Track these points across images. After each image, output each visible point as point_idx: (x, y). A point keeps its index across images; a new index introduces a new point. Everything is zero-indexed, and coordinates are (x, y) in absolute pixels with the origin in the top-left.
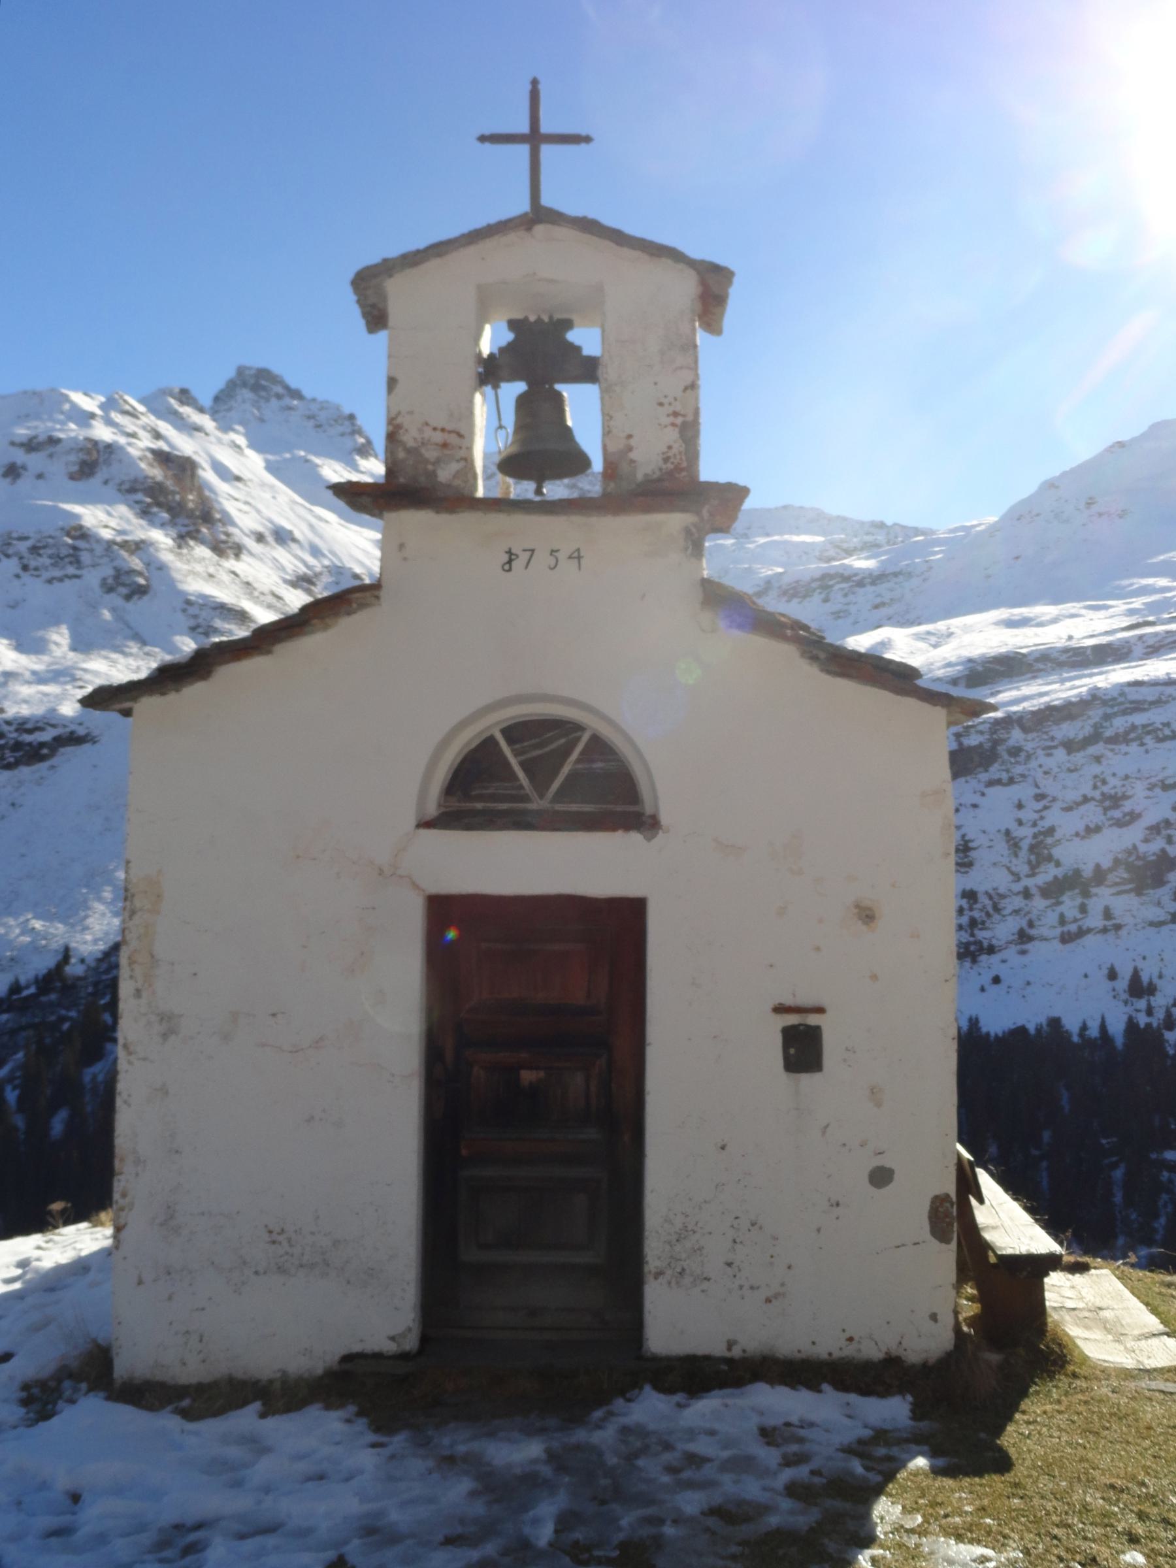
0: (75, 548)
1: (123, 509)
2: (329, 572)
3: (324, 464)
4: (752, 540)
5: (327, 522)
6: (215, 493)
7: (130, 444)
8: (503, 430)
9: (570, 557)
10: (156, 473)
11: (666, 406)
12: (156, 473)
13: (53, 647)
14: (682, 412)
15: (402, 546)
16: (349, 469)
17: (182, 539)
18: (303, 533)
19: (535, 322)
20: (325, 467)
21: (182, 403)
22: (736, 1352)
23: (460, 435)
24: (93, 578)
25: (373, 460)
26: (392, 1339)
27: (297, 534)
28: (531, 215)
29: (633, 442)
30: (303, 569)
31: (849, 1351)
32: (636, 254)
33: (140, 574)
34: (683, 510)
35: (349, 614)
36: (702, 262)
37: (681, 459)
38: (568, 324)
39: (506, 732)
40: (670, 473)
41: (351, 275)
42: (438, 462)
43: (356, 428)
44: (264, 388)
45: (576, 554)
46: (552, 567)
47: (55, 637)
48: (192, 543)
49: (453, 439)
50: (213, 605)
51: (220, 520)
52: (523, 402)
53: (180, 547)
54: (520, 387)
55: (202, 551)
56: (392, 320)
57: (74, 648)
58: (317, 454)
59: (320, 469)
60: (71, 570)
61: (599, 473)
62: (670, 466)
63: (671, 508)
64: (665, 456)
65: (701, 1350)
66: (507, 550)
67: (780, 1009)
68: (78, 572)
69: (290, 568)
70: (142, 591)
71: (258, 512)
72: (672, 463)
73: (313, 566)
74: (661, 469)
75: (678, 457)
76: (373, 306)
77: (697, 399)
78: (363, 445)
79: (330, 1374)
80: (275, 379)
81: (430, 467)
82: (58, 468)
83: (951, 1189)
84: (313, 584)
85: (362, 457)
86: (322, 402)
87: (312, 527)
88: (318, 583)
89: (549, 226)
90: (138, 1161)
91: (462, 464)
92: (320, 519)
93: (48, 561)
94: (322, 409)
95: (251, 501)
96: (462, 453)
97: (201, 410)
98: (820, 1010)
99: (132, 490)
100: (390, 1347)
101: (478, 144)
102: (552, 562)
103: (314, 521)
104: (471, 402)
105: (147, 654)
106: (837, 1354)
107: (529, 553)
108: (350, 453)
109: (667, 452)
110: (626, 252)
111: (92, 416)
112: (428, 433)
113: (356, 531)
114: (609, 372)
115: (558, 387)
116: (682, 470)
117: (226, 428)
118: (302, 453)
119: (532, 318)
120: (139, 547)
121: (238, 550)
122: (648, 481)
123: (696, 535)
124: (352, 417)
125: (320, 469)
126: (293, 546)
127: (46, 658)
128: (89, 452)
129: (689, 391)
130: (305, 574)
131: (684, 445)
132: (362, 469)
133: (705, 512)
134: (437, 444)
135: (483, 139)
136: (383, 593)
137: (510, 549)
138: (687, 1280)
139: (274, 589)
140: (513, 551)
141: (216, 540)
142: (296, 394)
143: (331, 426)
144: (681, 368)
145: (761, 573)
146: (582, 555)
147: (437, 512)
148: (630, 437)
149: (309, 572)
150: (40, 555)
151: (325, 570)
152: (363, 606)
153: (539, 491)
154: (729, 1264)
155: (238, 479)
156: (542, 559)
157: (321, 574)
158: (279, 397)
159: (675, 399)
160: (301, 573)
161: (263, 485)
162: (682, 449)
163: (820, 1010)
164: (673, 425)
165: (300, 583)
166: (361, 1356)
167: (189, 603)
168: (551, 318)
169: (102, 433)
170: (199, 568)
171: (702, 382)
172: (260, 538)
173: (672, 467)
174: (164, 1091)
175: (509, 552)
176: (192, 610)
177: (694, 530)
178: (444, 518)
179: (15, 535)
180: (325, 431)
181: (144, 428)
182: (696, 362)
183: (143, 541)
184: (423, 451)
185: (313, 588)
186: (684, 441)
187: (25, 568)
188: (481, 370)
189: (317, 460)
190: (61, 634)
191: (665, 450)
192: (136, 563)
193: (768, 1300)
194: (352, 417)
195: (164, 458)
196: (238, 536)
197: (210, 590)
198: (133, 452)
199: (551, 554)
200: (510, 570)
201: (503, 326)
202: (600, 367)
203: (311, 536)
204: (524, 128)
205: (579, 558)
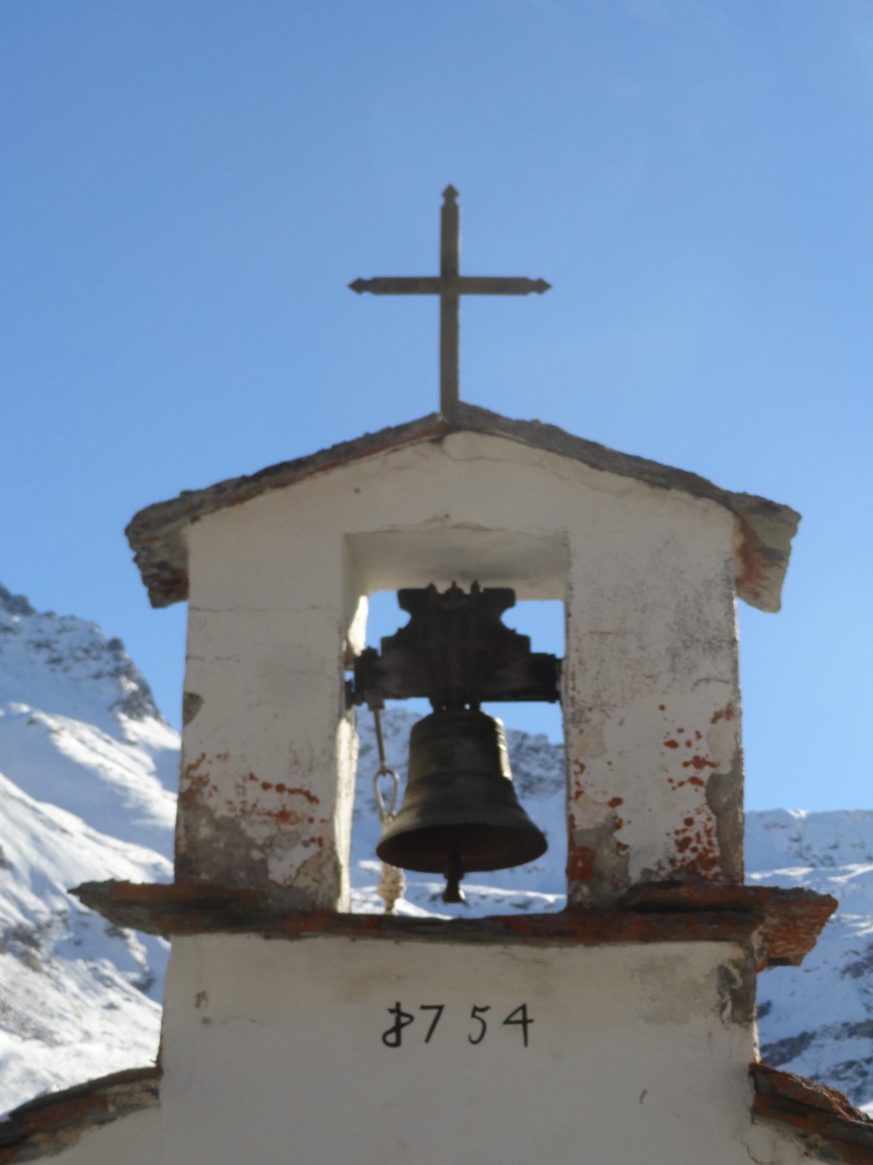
2: (65, 921)
3: (63, 729)
4: (841, 868)
5: (64, 831)
8: (388, 776)
9: (507, 1022)
11: (682, 747)
14: (711, 759)
15: (201, 997)
16: (107, 737)
18: (20, 851)
19: (449, 593)
20: (66, 734)
23: (312, 799)
25: (150, 720)
27: (10, 854)
28: (440, 419)
29: (621, 812)
30: (16, 917)
32: (629, 482)
35: (102, 1122)
36: (744, 497)
37: (710, 843)
38: (507, 599)
40: (691, 868)
41: (126, 518)
42: (269, 844)
43: (122, 664)
45: (519, 1016)
46: (475, 1037)
49: (298, 805)
56: (193, 590)
58: (51, 711)
59: (54, 736)
61: (558, 747)
63: (695, 936)
64: (681, 837)
66: (393, 1006)
72: (694, 850)
73: (36, 912)
74: (672, 861)
75: (704, 839)
76: (163, 565)
77: (737, 735)
78: (134, 694)
81: (256, 855)
84: (36, 945)
85: (131, 717)
86: (63, 619)
87: (35, 839)
88: (42, 942)
89: (472, 436)
91: (314, 848)
94: (62, 630)
96: (315, 830)
101: (352, 294)
102: (475, 1028)
103: (40, 829)
104: (333, 738)
107: (434, 1012)
108: (111, 709)
109: (684, 831)
110: (608, 478)
112: (253, 792)
113: (115, 849)
115: (488, 708)
116: (713, 862)
118: (25, 708)
119: (442, 588)
122: (648, 884)
123: (740, 982)
124: (115, 645)
125: (54, 736)
129: (721, 721)
130: (20, 926)
131: (714, 817)
132: (132, 738)
133: (756, 940)
134: (269, 814)
135: (359, 286)
136: (164, 1085)
137: (398, 1005)
140: (404, 1009)
142: (20, 605)
143: (77, 660)
144: (707, 680)
145: (861, 929)
146: (529, 1017)
147: (267, 937)
148: (616, 802)
149: (27, 922)
151: (57, 918)
152: (125, 1109)
153: (451, 895)
157: (49, 925)
159: (699, 736)
160: (13, 923)
162: (711, 825)
164: (695, 781)
165: (11, 942)
168: (475, 587)
171: (746, 705)
173: (692, 856)
175: (397, 1011)
177: (735, 973)
178: (281, 947)
180: (66, 670)
182: (735, 669)
184: (244, 825)
185: (33, 951)
186: (715, 811)
188: (349, 675)
189: (51, 722)
191: (681, 826)
194: (115, 645)
199: (473, 1016)
200: (398, 1043)
201: (390, 598)
202: (563, 678)
203: (33, 856)
204: (432, 269)
205: (525, 1022)
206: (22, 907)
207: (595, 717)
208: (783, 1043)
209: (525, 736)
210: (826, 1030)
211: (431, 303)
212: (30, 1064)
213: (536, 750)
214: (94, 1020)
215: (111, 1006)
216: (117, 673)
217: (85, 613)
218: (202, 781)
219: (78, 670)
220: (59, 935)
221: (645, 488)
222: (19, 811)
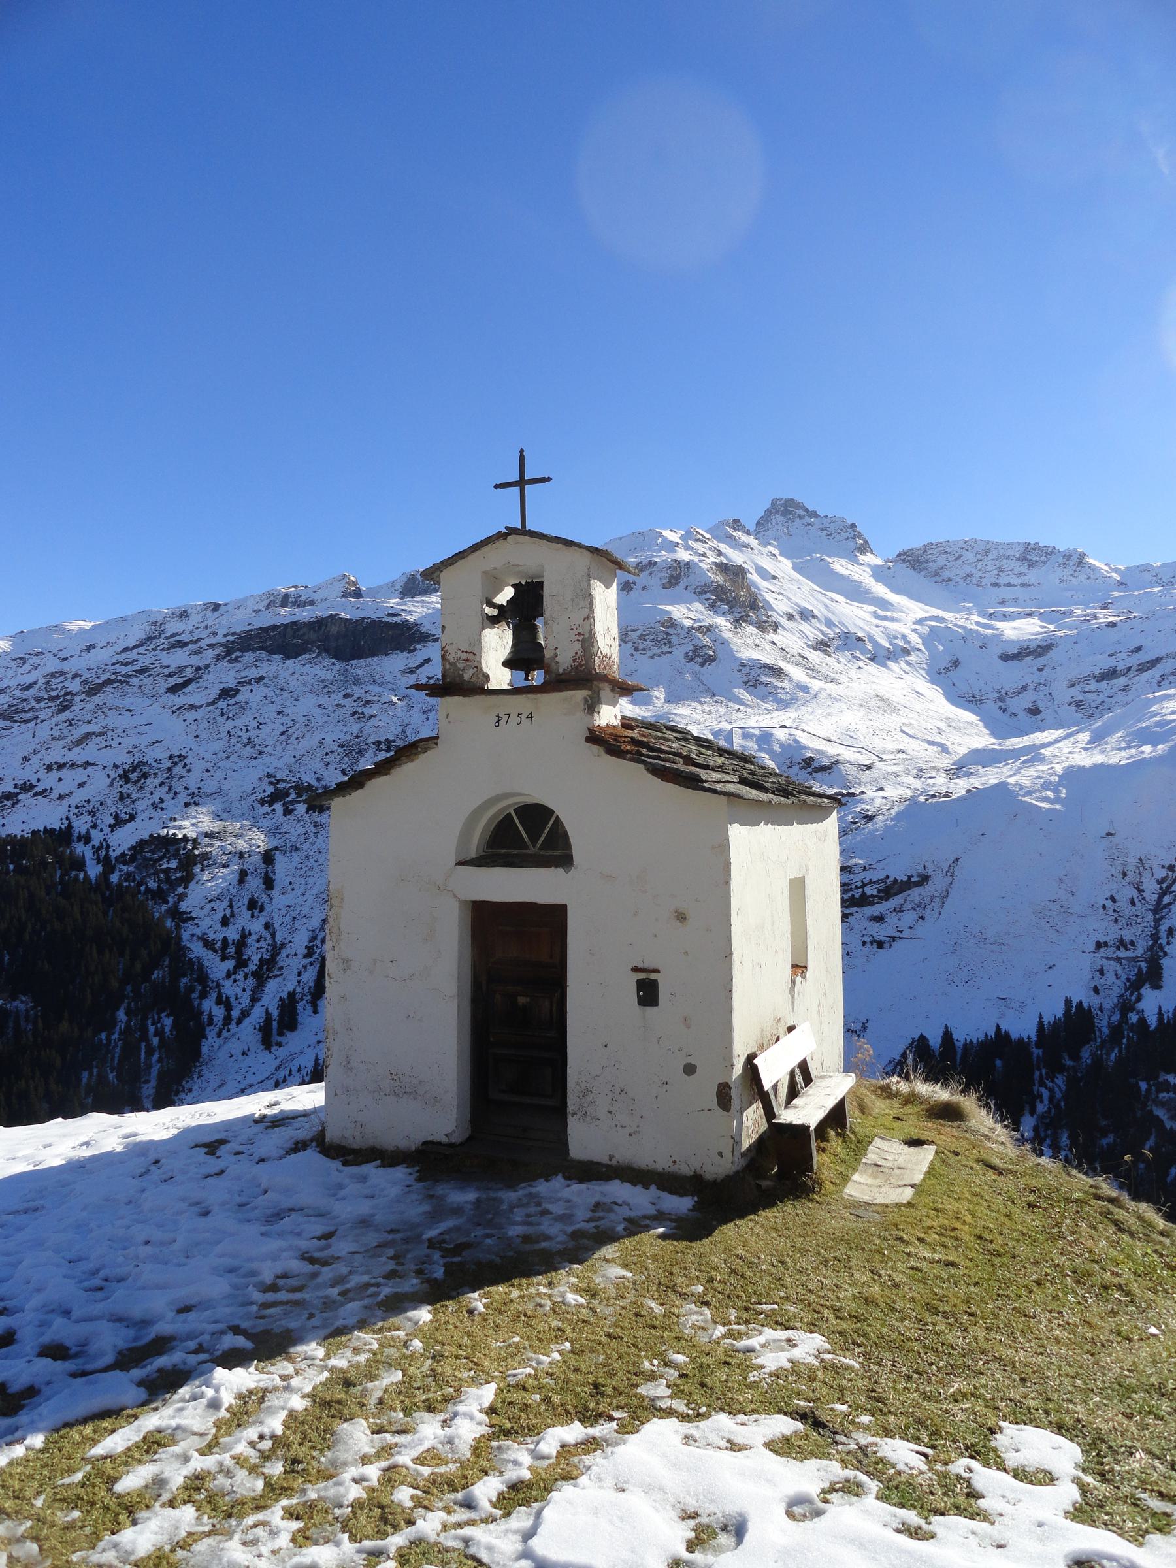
0: (668, 634)
1: (698, 605)
6: (759, 590)
7: (700, 561)
10: (719, 579)
12: (719, 579)
13: (655, 700)
15: (448, 715)
17: (737, 622)
18: (820, 612)
21: (735, 529)
22: (614, 1162)
24: (679, 653)
26: (446, 1135)
27: (816, 612)
29: (558, 652)
31: (674, 1169)
33: (710, 648)
34: (585, 689)
40: (576, 668)
44: (791, 512)
47: (656, 694)
48: (744, 624)
49: (471, 656)
50: (759, 666)
51: (762, 607)
53: (736, 628)
55: (751, 629)
57: (668, 701)
58: (829, 556)
60: (665, 649)
62: (576, 664)
65: (596, 1158)
67: (636, 969)
68: (670, 650)
69: (811, 636)
70: (712, 659)
71: (789, 599)
79: (417, 1151)
80: (799, 505)
82: (655, 581)
84: (829, 647)
90: (335, 1033)
92: (832, 600)
93: (651, 644)
95: (782, 591)
96: (476, 664)
97: (748, 533)
98: (657, 971)
99: (703, 592)
100: (445, 1140)
103: (827, 602)
105: (716, 702)
106: (667, 1169)
111: (677, 544)
117: (765, 544)
120: (709, 629)
121: (776, 627)
124: (853, 526)
126: (813, 620)
127: (651, 708)
128: (675, 569)
138: (588, 1119)
139: (801, 652)
141: (760, 621)
142: (814, 514)
148: (556, 648)
150: (645, 640)
154: (610, 1112)
155: (774, 577)
156: (514, 718)
158: (801, 517)
161: (791, 580)
163: (657, 971)
166: (431, 1142)
167: (742, 665)
169: (683, 555)
170: (749, 641)
172: (790, 617)
174: (344, 998)
176: (744, 671)
179: (629, 628)
181: (710, 549)
183: (711, 626)
187: (636, 649)
190: (660, 692)
192: (707, 641)
193: (631, 1135)
194: (853, 526)
195: (723, 568)
196: (775, 617)
197: (756, 655)
198: (704, 566)
203: (826, 612)
206: (823, 633)
207: (551, 622)
208: (1148, 662)
209: (1029, 544)
210: (1168, 655)
211: (518, 489)
212: (829, 692)
213: (1035, 550)
214: (853, 673)
215: (860, 668)
216: (854, 537)
217: (840, 515)
218: (446, 651)
219: (838, 538)
220: (836, 642)
221: (564, 547)
222: (819, 596)
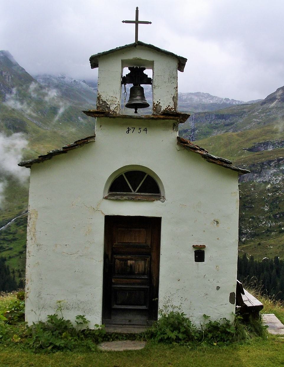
39: (125, 174)
52: (132, 90)
54: (132, 85)
83: (235, 290)
114: (155, 83)
115: (142, 85)
153: (136, 112)
200: (128, 133)
